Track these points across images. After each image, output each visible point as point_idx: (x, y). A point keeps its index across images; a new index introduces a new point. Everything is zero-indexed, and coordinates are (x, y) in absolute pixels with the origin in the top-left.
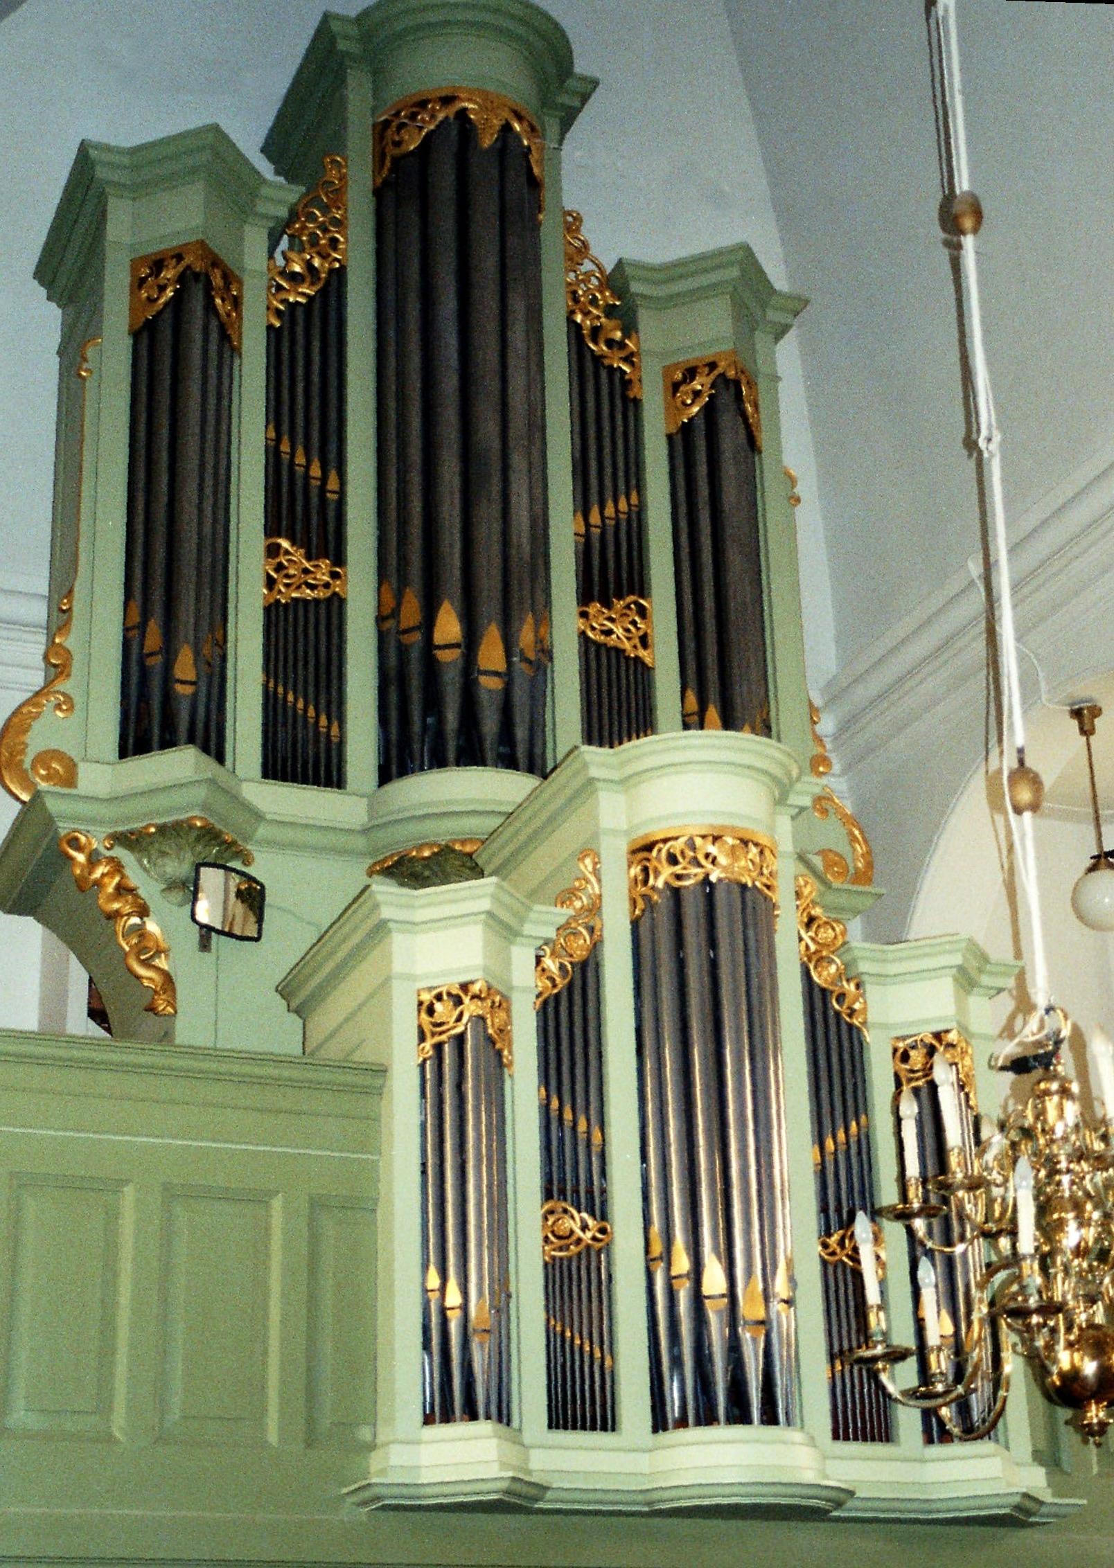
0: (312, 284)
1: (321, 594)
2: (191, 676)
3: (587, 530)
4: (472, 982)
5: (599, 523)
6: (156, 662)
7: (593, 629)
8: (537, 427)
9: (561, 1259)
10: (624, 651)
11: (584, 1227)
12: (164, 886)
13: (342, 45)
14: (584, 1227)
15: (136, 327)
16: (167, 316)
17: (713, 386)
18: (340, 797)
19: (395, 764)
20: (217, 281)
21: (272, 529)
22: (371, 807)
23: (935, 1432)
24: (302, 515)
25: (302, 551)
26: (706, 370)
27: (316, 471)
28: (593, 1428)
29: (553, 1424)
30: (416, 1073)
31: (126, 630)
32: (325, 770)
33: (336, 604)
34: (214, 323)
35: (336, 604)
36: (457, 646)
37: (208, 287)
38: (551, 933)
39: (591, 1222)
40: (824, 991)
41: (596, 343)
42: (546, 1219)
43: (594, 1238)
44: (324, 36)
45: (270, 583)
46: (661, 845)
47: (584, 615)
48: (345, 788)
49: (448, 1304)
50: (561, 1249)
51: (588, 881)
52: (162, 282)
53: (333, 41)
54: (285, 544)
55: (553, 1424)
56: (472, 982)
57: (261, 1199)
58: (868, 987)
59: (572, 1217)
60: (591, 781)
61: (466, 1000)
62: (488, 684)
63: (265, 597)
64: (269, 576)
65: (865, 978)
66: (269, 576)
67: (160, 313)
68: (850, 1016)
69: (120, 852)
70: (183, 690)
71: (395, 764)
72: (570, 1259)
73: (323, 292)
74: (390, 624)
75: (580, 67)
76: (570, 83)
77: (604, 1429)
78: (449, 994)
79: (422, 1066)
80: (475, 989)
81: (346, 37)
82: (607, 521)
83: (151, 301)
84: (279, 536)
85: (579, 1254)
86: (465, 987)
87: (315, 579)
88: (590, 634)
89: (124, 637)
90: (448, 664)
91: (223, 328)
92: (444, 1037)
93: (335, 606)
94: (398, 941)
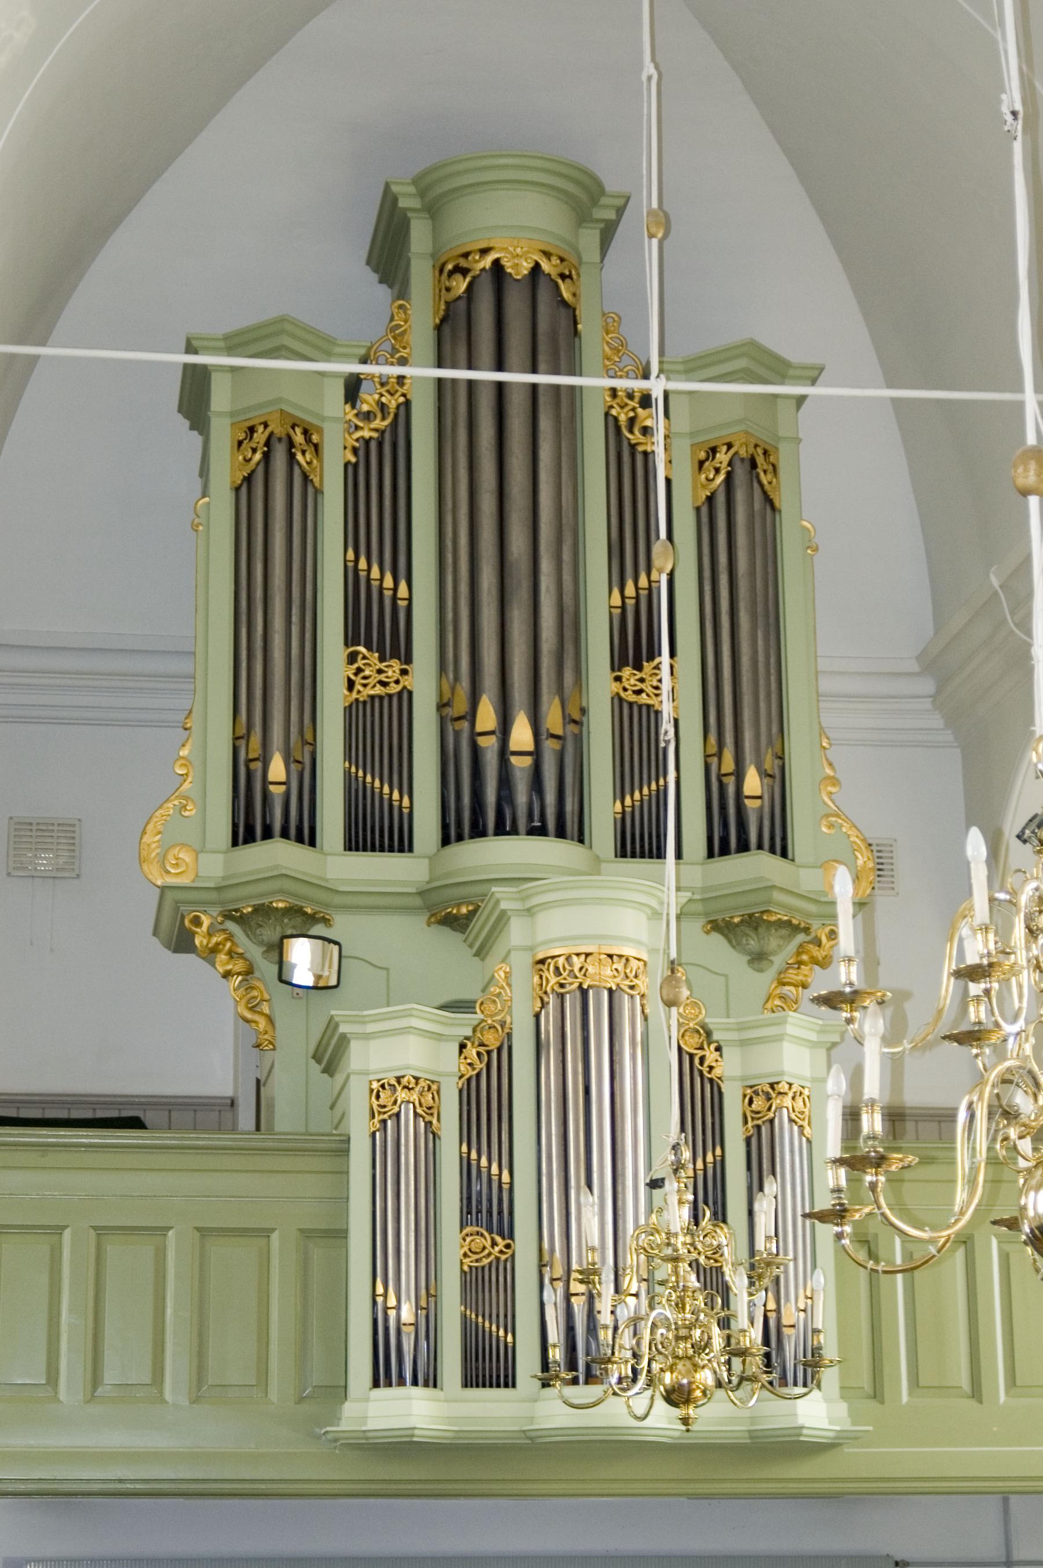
0: (383, 419)
1: (394, 689)
2: (283, 777)
3: (623, 602)
4: (403, 1077)
5: (634, 594)
6: (257, 766)
7: (625, 689)
8: (570, 529)
9: (477, 1268)
10: (653, 706)
11: (494, 1244)
12: (265, 948)
13: (402, 203)
14: (494, 1244)
15: (236, 485)
16: (260, 470)
17: (730, 464)
18: (410, 860)
19: (450, 835)
20: (299, 438)
21: (351, 638)
22: (431, 869)
23: (473, 1378)
24: (376, 627)
25: (376, 655)
26: (725, 448)
27: (388, 582)
28: (498, 1386)
29: (467, 1383)
30: (368, 1142)
31: (236, 739)
32: (397, 838)
33: (405, 696)
34: (297, 471)
35: (405, 696)
36: (492, 733)
37: (291, 444)
38: (468, 1032)
39: (498, 1239)
40: (692, 1056)
41: (631, 432)
42: (464, 1240)
43: (501, 1252)
44: (389, 200)
45: (351, 685)
46: (549, 960)
47: (618, 679)
48: (411, 849)
49: (389, 1305)
50: (477, 1261)
51: (503, 988)
52: (254, 445)
53: (395, 200)
54: (362, 649)
55: (467, 1383)
56: (403, 1077)
57: (266, 1233)
58: (725, 1050)
59: (485, 1238)
60: (504, 912)
61: (399, 1088)
62: (521, 764)
63: (346, 696)
64: (349, 680)
65: (722, 1043)
66: (349, 680)
67: (253, 471)
68: (709, 1072)
69: (231, 925)
70: (277, 790)
71: (450, 835)
72: (483, 1268)
73: (395, 424)
74: (447, 711)
75: (611, 185)
76: (604, 201)
77: (506, 1386)
78: (390, 1085)
79: (373, 1134)
80: (404, 1081)
81: (405, 195)
82: (641, 592)
83: (248, 461)
84: (359, 645)
85: (490, 1264)
86: (398, 1079)
87: (387, 677)
88: (623, 694)
89: (234, 745)
90: (487, 748)
91: (305, 477)
92: (385, 1116)
93: (406, 696)
94: (355, 1047)
